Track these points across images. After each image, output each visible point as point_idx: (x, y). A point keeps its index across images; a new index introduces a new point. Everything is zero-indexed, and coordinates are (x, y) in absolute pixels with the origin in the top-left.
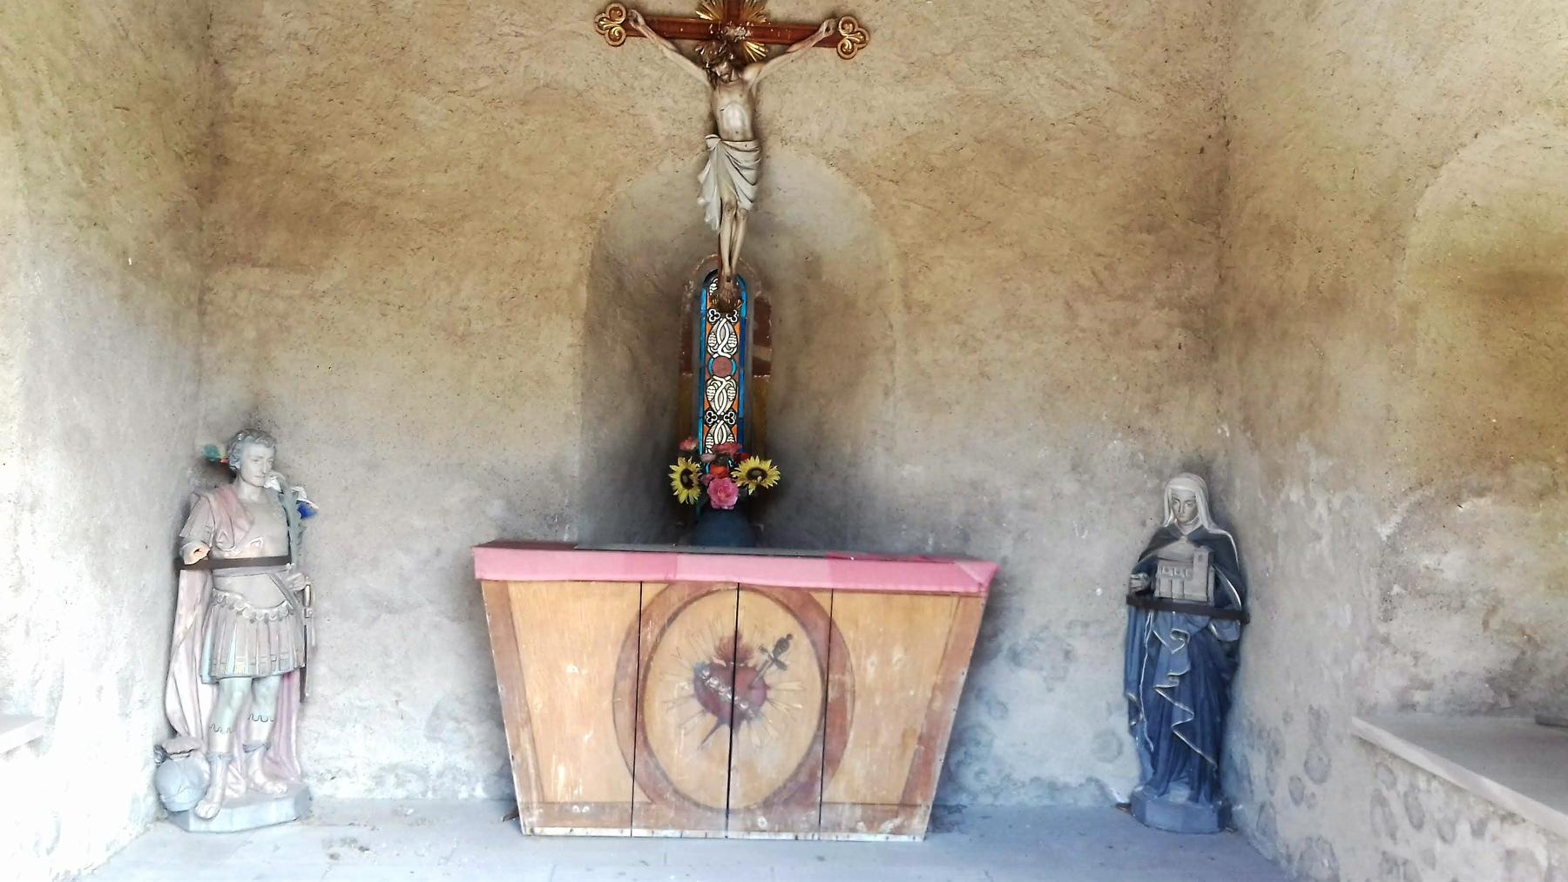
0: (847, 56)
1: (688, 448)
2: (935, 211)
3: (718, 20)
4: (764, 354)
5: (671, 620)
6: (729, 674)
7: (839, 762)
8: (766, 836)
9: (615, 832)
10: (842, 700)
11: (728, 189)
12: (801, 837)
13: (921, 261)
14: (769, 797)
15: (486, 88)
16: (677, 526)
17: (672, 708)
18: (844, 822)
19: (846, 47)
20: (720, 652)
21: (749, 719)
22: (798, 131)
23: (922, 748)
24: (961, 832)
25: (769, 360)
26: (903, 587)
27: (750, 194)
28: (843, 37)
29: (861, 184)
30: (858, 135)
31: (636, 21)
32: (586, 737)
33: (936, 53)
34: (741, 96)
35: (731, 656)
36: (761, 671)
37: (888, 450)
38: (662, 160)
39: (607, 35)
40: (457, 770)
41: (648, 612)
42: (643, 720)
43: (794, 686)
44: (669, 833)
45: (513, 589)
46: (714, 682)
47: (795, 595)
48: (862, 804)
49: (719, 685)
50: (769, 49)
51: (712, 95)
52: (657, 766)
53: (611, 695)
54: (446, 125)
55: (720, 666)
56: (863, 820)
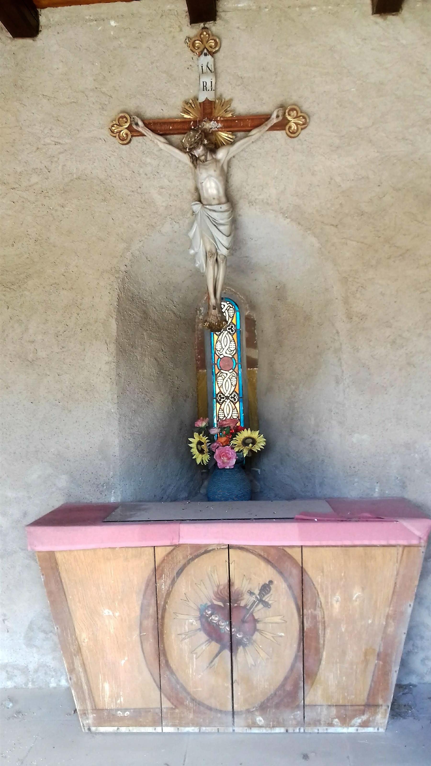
0: (293, 135)
1: (200, 425)
2: (366, 244)
3: (197, 118)
4: (254, 354)
5: (179, 574)
6: (227, 611)
7: (316, 674)
8: (263, 730)
9: (150, 730)
10: (315, 629)
11: (209, 241)
12: (291, 730)
13: (358, 283)
14: (264, 702)
15: (37, 183)
16: (202, 473)
17: (184, 639)
18: (323, 719)
19: (292, 129)
20: (218, 596)
21: (245, 645)
22: (260, 194)
23: (381, 663)
24: (415, 717)
25: (257, 357)
26: (357, 543)
27: (226, 244)
28: (289, 121)
29: (310, 229)
30: (305, 193)
31: (137, 124)
32: (123, 662)
33: (361, 127)
34: (215, 171)
35: (227, 599)
36: (251, 608)
37: (341, 423)
38: (163, 225)
39: (117, 137)
40: (47, 667)
41: (161, 568)
42: (164, 647)
43: (277, 619)
44: (190, 729)
45: (59, 556)
46: (215, 619)
47: (273, 551)
48: (336, 706)
49: (219, 621)
50: (235, 135)
51: (195, 172)
52: (178, 682)
53: (138, 630)
54: (10, 212)
55: (220, 606)
56: (338, 717)
